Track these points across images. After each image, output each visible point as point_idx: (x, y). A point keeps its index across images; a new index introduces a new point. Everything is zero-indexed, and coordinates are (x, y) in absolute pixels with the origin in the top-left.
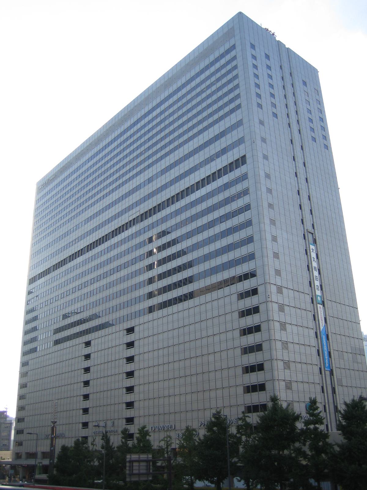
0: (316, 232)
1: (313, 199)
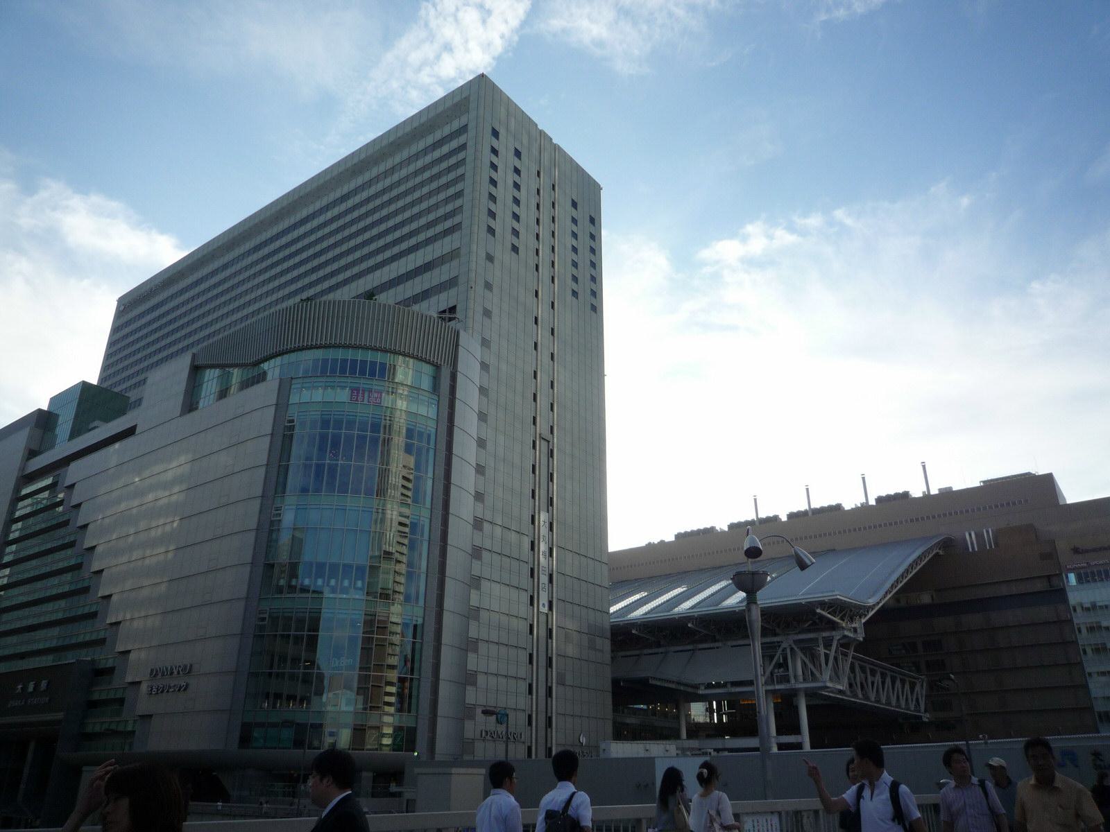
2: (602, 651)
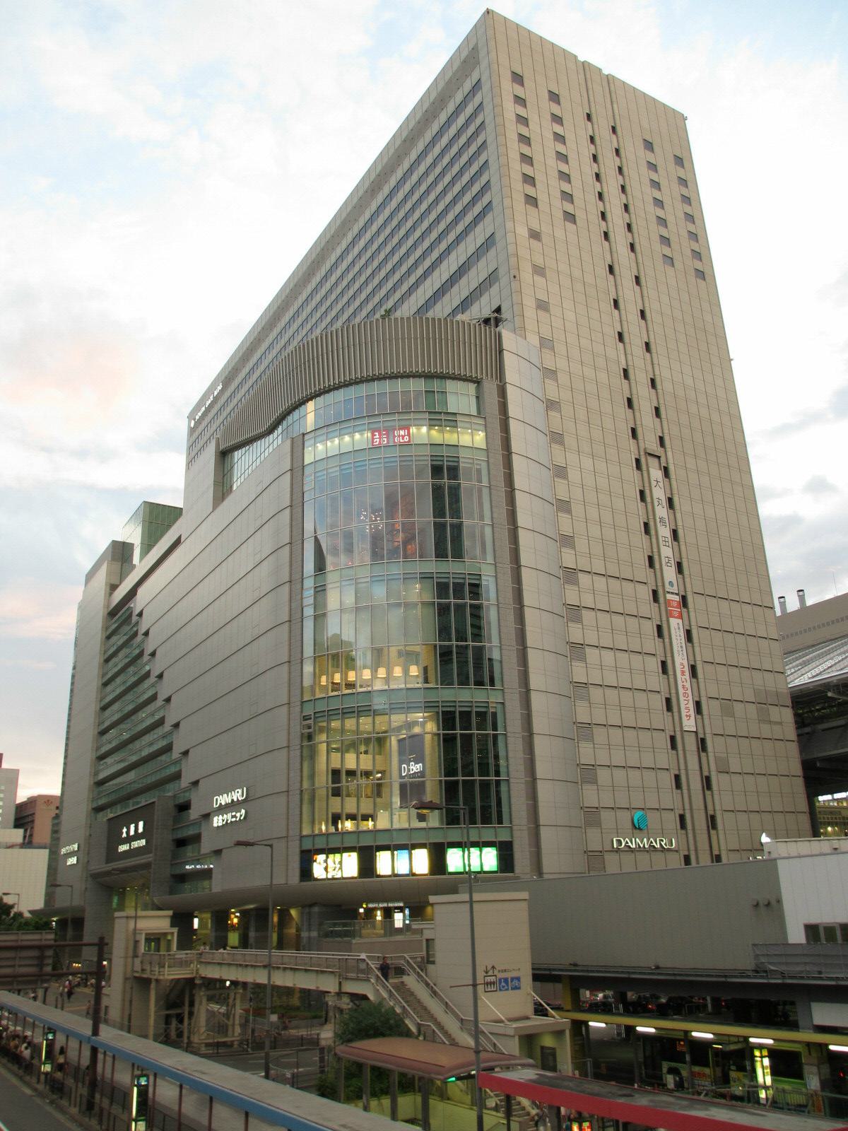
0: (670, 454)
1: (665, 385)
2: (780, 723)
